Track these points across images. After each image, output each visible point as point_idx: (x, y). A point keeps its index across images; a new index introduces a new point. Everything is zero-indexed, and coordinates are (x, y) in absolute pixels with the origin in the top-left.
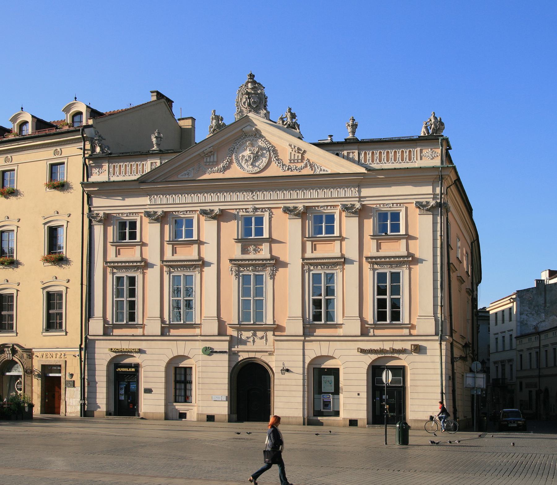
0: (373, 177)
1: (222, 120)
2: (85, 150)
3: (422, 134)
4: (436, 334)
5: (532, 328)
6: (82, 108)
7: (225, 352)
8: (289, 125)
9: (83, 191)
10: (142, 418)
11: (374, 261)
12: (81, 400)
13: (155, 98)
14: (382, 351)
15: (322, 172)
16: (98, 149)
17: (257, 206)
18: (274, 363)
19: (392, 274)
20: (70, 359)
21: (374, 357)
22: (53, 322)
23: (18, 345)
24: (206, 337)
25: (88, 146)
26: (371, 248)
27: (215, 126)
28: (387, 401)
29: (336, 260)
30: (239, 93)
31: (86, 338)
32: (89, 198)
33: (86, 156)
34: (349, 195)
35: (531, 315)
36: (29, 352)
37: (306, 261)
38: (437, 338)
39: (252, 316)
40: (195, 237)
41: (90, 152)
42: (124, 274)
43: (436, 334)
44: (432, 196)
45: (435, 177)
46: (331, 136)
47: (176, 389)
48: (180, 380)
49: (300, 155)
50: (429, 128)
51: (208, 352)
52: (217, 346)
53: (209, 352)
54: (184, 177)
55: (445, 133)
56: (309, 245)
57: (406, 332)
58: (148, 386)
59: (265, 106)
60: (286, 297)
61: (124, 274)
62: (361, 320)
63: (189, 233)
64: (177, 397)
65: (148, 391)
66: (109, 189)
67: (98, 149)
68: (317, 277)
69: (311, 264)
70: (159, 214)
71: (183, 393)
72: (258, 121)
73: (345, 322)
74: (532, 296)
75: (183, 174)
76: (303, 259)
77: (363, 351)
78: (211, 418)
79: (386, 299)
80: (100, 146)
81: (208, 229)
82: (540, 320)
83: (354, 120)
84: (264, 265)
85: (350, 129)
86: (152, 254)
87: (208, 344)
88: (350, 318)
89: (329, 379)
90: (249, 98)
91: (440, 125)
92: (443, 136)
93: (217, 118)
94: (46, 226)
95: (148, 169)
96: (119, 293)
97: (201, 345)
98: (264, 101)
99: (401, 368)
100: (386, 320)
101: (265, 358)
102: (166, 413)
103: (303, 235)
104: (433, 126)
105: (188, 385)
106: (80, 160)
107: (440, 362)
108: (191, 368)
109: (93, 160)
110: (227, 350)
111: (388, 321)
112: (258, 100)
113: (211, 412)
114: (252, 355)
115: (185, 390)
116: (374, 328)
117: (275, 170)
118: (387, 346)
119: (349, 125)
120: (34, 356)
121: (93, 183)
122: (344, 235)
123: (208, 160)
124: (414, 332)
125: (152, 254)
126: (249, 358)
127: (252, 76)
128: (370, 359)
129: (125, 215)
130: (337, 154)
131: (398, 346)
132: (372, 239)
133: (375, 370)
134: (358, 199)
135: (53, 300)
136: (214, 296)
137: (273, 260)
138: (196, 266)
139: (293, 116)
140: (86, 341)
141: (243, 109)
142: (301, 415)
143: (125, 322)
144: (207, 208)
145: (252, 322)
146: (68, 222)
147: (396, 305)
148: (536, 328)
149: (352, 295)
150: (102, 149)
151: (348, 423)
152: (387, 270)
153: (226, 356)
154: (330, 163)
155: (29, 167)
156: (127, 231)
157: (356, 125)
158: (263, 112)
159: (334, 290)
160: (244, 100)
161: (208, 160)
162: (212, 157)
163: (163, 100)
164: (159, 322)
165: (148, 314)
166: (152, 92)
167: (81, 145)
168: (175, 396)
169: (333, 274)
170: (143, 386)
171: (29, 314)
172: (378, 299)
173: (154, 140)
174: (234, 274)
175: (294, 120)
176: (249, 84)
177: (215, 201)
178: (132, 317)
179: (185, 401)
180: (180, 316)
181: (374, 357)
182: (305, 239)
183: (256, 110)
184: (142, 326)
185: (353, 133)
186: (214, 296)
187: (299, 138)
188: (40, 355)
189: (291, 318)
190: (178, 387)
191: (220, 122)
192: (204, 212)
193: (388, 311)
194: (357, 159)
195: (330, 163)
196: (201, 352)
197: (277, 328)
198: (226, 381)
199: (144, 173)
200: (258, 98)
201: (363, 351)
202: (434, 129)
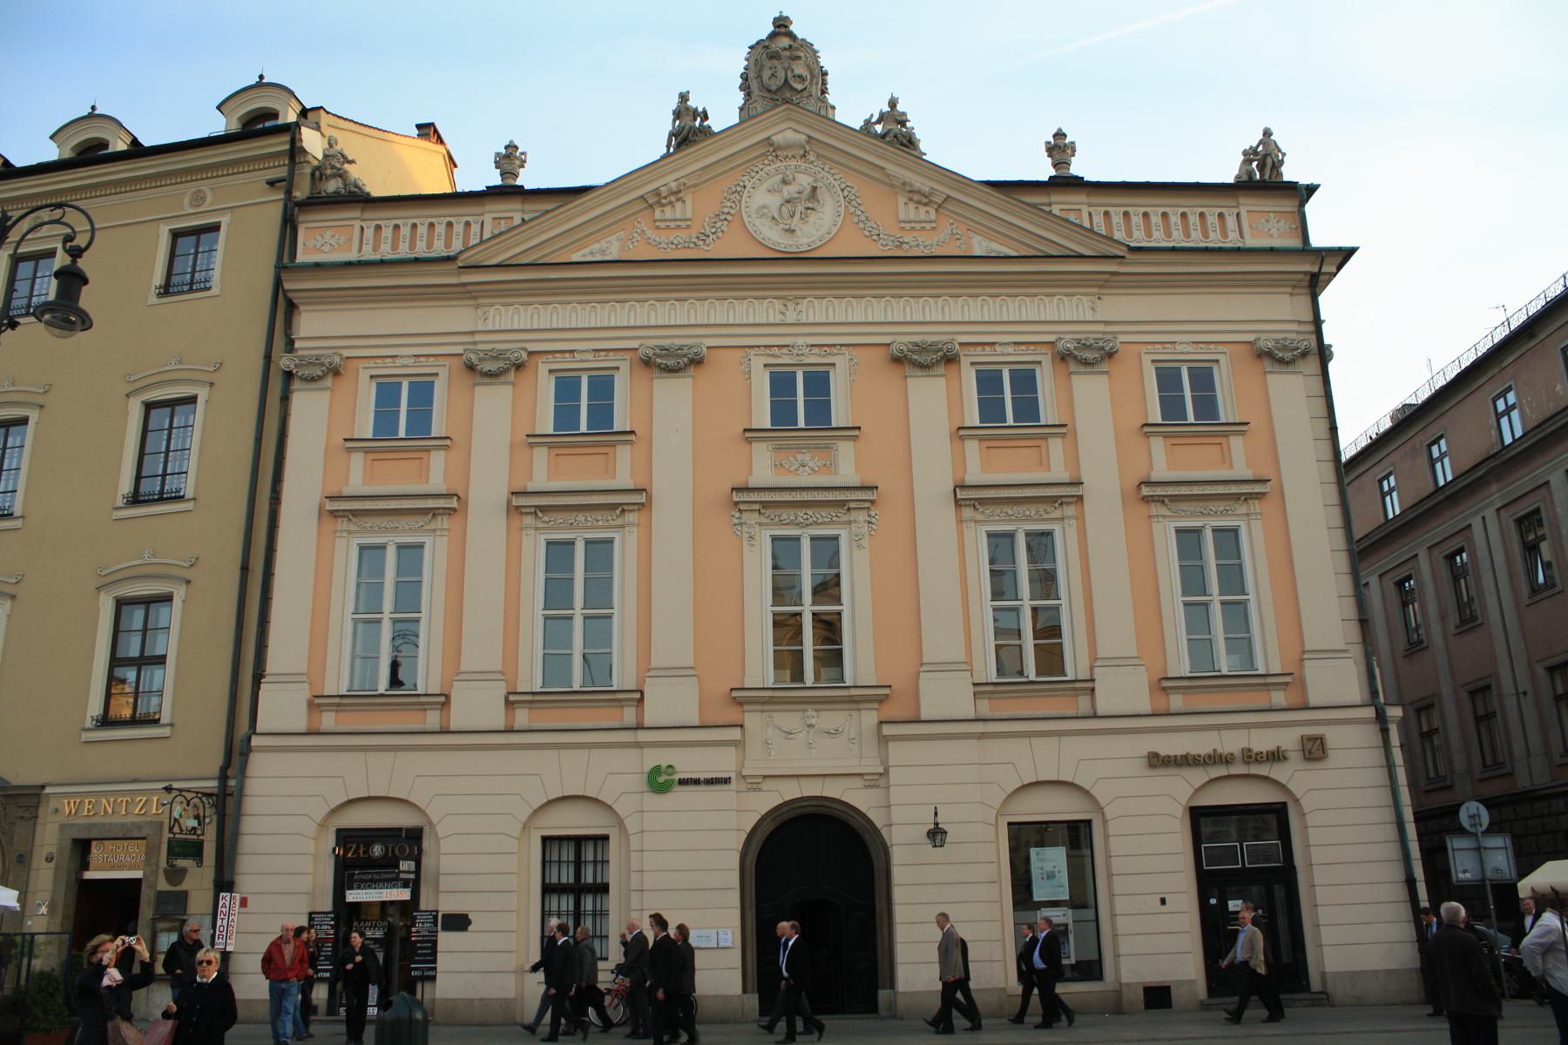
1: (705, 117)
59: (824, 92)
60: (926, 599)
61: (392, 538)
77: (1156, 761)
87: (662, 758)
89: (1050, 862)
106: (275, 213)
113: (1154, 977)
118: (1232, 743)
128: (1182, 789)
131: (1262, 742)
181: (1198, 776)
184: (1088, 687)
201: (1156, 761)
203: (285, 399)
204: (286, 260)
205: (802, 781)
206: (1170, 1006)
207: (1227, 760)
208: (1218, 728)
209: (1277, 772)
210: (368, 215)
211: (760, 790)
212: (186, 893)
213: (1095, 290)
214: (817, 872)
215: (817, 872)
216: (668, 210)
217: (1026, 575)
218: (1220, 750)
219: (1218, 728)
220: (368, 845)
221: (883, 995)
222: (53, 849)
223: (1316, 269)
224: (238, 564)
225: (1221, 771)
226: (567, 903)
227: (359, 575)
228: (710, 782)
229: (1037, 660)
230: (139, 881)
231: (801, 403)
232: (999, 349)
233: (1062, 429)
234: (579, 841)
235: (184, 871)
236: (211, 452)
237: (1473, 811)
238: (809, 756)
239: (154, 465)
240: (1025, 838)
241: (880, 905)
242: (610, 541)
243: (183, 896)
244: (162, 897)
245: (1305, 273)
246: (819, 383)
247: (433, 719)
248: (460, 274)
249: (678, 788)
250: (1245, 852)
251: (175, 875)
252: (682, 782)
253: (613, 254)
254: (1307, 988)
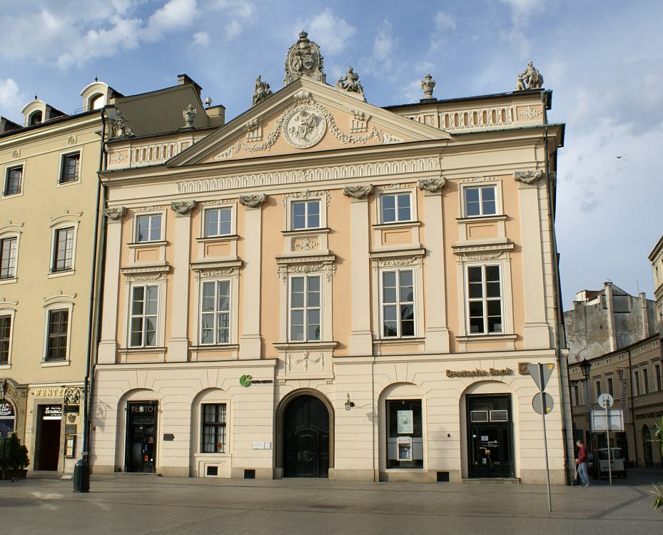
1: (268, 87)
7: (270, 382)
8: (351, 87)
9: (100, 182)
10: (160, 475)
12: (84, 451)
14: (478, 373)
15: (393, 142)
16: (119, 133)
17: (311, 189)
18: (334, 395)
19: (488, 268)
20: (522, 391)
21: (469, 381)
22: (56, 350)
23: (9, 379)
26: (461, 236)
28: (489, 441)
32: (106, 189)
34: (428, 166)
36: (24, 389)
37: (374, 256)
38: (553, 352)
39: (306, 331)
40: (233, 232)
42: (482, 263)
44: (535, 165)
48: (211, 422)
49: (365, 123)
51: (450, 374)
52: (257, 374)
53: (246, 381)
55: (546, 86)
57: (510, 345)
60: (352, 304)
61: (215, 279)
63: (226, 227)
64: (206, 446)
65: (169, 437)
67: (119, 133)
68: (388, 277)
69: (381, 259)
70: (119, 211)
71: (213, 441)
76: (371, 253)
77: (451, 374)
78: (250, 474)
79: (481, 303)
84: (321, 262)
86: (432, 237)
87: (247, 372)
89: (405, 417)
93: (264, 86)
96: (208, 305)
99: (506, 397)
102: (116, 467)
105: (221, 430)
106: (98, 146)
108: (224, 405)
109: (110, 143)
110: (273, 379)
111: (399, 336)
113: (250, 466)
114: (304, 385)
117: (332, 143)
118: (486, 366)
120: (29, 394)
121: (112, 171)
123: (251, 136)
124: (523, 344)
125: (432, 237)
128: (462, 384)
129: (148, 209)
131: (500, 366)
133: (472, 401)
134: (440, 173)
135: (58, 321)
136: (257, 306)
137: (332, 255)
139: (355, 79)
144: (249, 195)
145: (215, 343)
147: (495, 308)
149: (440, 300)
150: (124, 132)
151: (435, 477)
153: (270, 387)
154: (396, 130)
155: (41, 158)
158: (317, 73)
160: (295, 62)
162: (256, 131)
165: (245, 331)
167: (100, 128)
169: (228, 282)
170: (162, 430)
171: (28, 338)
172: (133, 319)
173: (187, 117)
174: (281, 278)
175: (356, 82)
177: (256, 183)
178: (224, 334)
179: (216, 451)
180: (214, 336)
181: (469, 381)
184: (237, 347)
186: (257, 306)
188: (36, 392)
190: (207, 432)
191: (266, 90)
192: (244, 201)
193: (485, 318)
194: (437, 126)
195: (396, 130)
196: (239, 383)
198: (271, 421)
200: (312, 58)
201: (451, 374)
203: (105, 228)
206: (448, 481)
207: (484, 374)
208: (480, 359)
214: (303, 430)
215: (303, 430)
217: (216, 301)
219: (480, 359)
220: (138, 407)
221: (330, 470)
222: (32, 408)
224: (90, 297)
225: (480, 379)
228: (264, 382)
229: (214, 336)
231: (304, 217)
232: (394, 187)
233: (420, 224)
235: (75, 417)
236: (80, 252)
237: (606, 398)
238: (304, 372)
239: (60, 256)
241: (280, 436)
242: (411, 271)
244: (67, 427)
246: (489, 193)
247: (161, 357)
249: (253, 384)
250: (490, 415)
252: (254, 382)
254: (514, 476)
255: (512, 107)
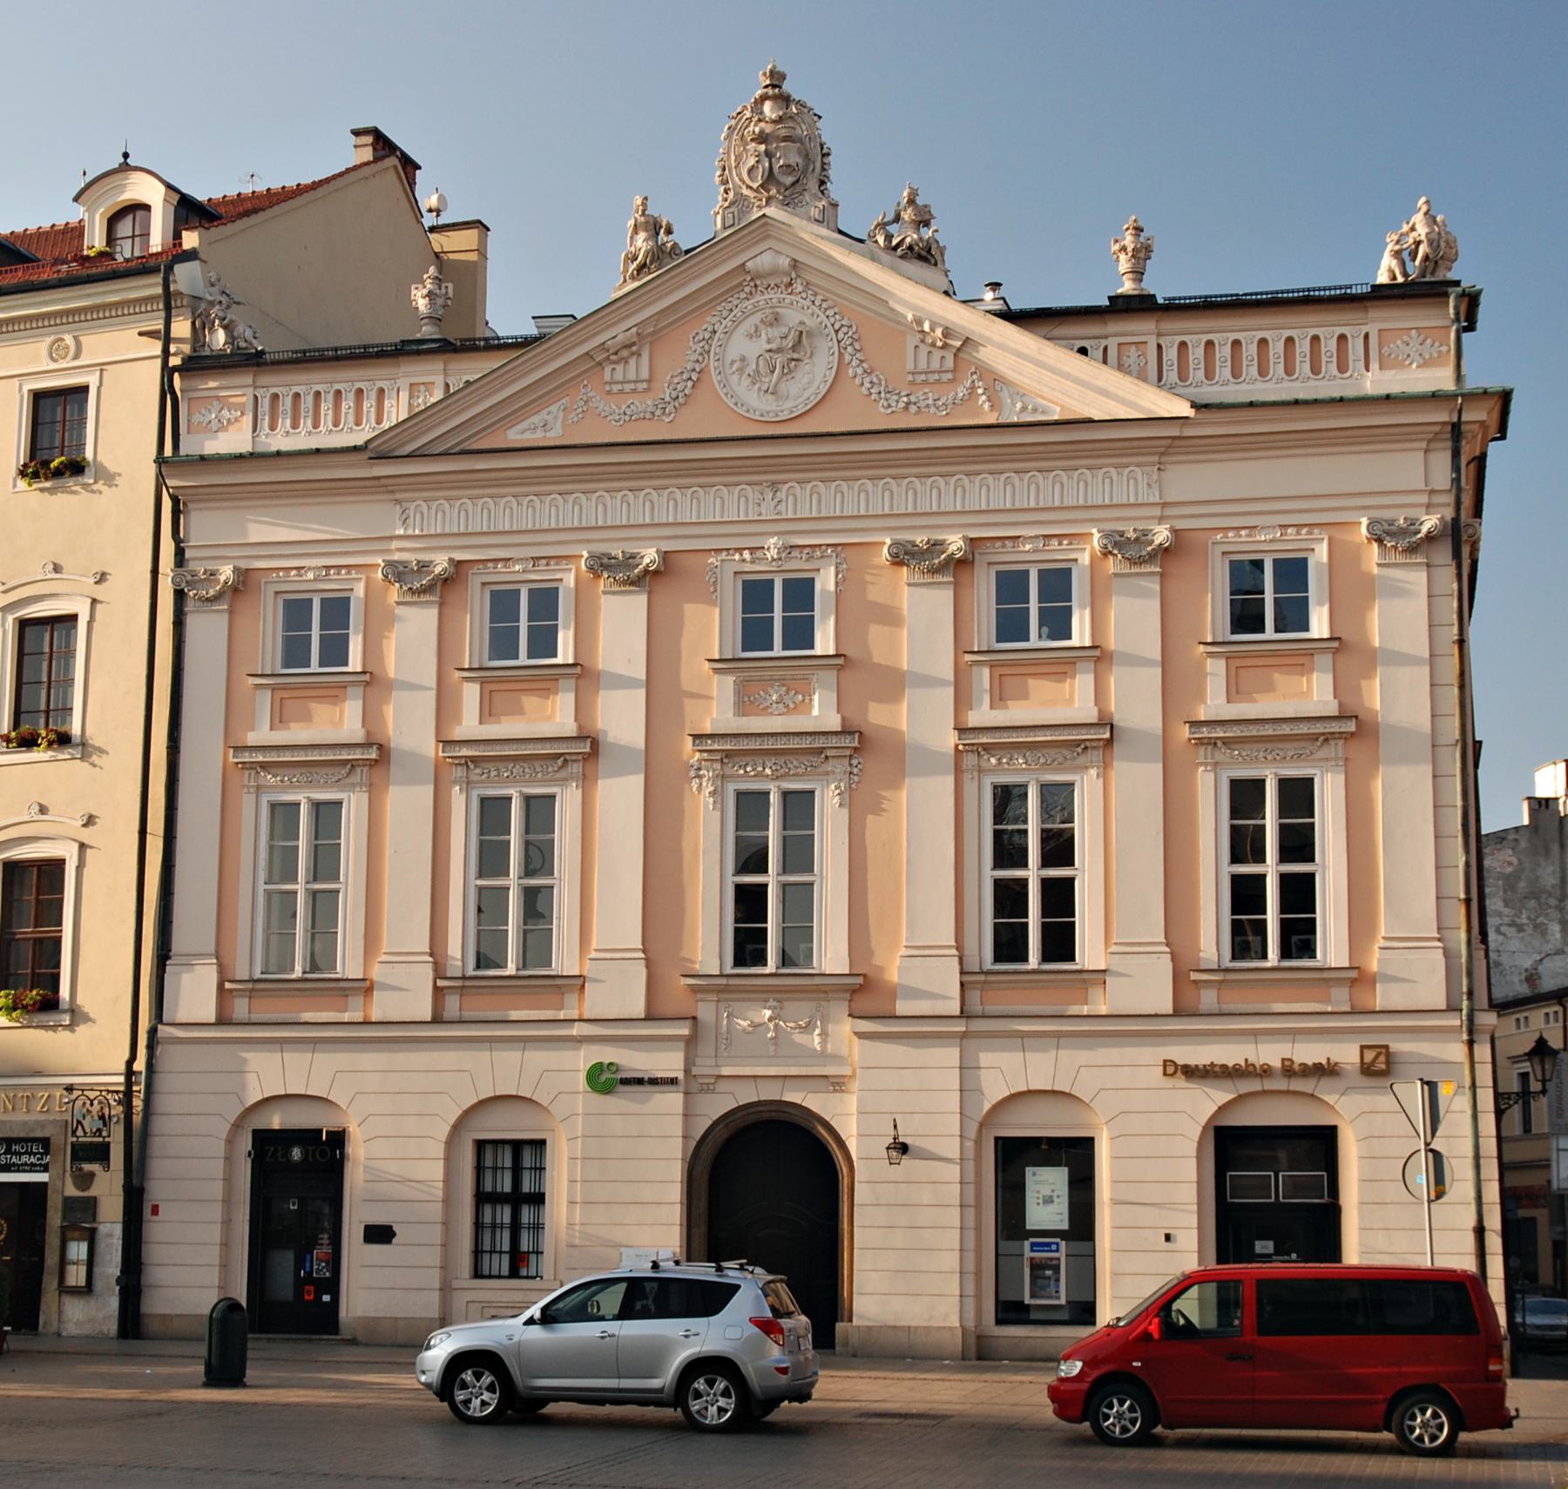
0: (1222, 428)
2: (167, 340)
3: (1383, 278)
4: (1452, 1008)
5: (1516, 979)
6: (148, 191)
7: (673, 1081)
8: (910, 248)
11: (1216, 738)
13: (367, 154)
16: (220, 338)
18: (851, 1122)
19: (1285, 784)
24: (612, 1028)
25: (182, 328)
26: (717, 709)
27: (647, 253)
29: (1320, 728)
30: (728, 137)
31: (153, 1032)
33: (175, 361)
35: (1511, 931)
38: (1454, 1021)
41: (187, 348)
43: (1452, 1008)
45: (1437, 428)
46: (995, 286)
47: (478, 1226)
50: (1405, 255)
53: (605, 1080)
54: (527, 435)
56: (471, 694)
57: (1340, 998)
58: (378, 1218)
59: (822, 183)
62: (435, 963)
65: (379, 1234)
66: (260, 475)
70: (438, 570)
72: (803, 228)
73: (1116, 964)
74: (1515, 861)
75: (525, 425)
77: (1172, 1069)
79: (1023, 883)
80: (225, 328)
81: (620, 627)
82: (1548, 948)
83: (1138, 230)
85: (1124, 264)
87: (607, 1054)
88: (1135, 948)
90: (768, 154)
91: (1441, 251)
92: (1457, 283)
93: (654, 227)
94: (10, 619)
95: (396, 411)
97: (583, 1059)
98: (818, 165)
100: (1025, 959)
101: (813, 1101)
103: (960, 648)
104: (1422, 250)
107: (1469, 1112)
110: (681, 1075)
112: (794, 163)
114: (769, 1093)
115: (515, 1228)
116: (251, 994)
118: (1270, 1054)
119: (1124, 249)
122: (1112, 643)
123: (619, 376)
126: (759, 1103)
127: (776, 79)
128: (1207, 1102)
130: (1083, 351)
131: (1309, 1053)
132: (716, 670)
137: (851, 733)
138: (565, 760)
140: (151, 1047)
141: (745, 192)
142: (955, 1322)
143: (298, 972)
146: (94, 601)
148: (1531, 978)
150: (231, 338)
152: (1031, 778)
154: (1056, 380)
156: (317, 633)
157: (1148, 249)
159: (1026, 850)
161: (619, 376)
162: (632, 362)
163: (393, 161)
164: (428, 971)
166: (356, 133)
168: (477, 1252)
175: (927, 233)
176: (767, 107)
177: (644, 520)
179: (514, 1273)
182: (968, 657)
183: (791, 196)
185: (1138, 274)
187: (946, 293)
189: (922, 952)
193: (1273, 914)
197: (862, 992)
199: (386, 425)
202: (1426, 258)
204: (168, 451)
205: (760, 1082)
207: (1266, 1072)
209: (1328, 1093)
210: (264, 379)
211: (713, 1091)
212: (94, 1200)
213: (1155, 458)
215: (770, 1190)
216: (620, 368)
218: (1252, 1060)
223: (1455, 419)
226: (526, 1188)
227: (272, 837)
230: (44, 1185)
231: (774, 617)
234: (517, 1146)
235: (92, 1175)
240: (1015, 1157)
243: (92, 1203)
244: (69, 1203)
245: (1444, 423)
248: (371, 466)
250: (1279, 1184)
251: (85, 1180)
252: (626, 1082)
253: (554, 436)
255: (1365, 329)
